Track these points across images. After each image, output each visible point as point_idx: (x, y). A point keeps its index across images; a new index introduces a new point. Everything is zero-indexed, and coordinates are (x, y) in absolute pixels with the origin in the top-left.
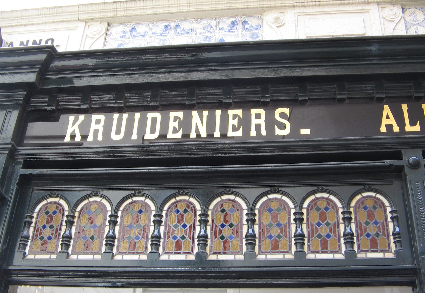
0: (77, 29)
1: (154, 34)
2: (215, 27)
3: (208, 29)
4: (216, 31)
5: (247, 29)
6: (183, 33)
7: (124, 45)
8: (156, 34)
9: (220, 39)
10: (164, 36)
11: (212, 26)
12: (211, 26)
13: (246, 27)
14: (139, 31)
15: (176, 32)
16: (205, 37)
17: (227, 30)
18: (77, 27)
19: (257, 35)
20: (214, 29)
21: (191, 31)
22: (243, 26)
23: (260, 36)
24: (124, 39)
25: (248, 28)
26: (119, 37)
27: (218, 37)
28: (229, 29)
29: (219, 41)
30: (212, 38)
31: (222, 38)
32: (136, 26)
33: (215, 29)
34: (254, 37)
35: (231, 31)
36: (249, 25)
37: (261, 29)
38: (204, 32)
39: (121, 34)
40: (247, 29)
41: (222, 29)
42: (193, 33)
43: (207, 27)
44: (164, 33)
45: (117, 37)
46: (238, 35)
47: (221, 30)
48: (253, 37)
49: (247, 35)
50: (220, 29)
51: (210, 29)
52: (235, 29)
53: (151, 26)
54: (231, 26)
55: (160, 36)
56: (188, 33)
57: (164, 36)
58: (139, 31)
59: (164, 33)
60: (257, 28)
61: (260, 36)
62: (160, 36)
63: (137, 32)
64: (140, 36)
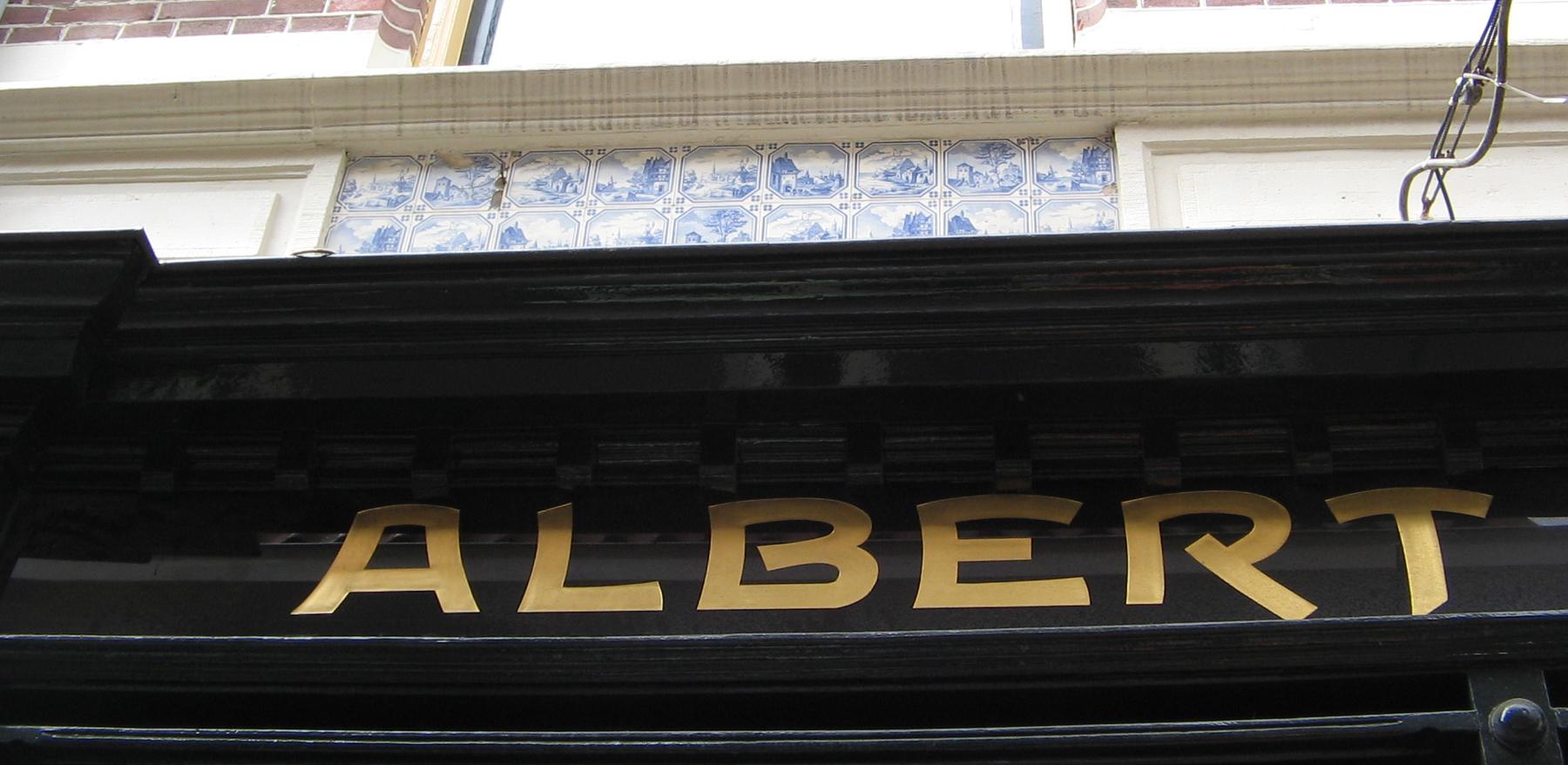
0: (305, 177)
1: (603, 194)
2: (582, 181)
3: (554, 187)
4: (584, 199)
5: (787, 188)
6: (806, 192)
7: (929, 222)
8: (614, 194)
9: (506, 231)
10: (644, 200)
11: (918, 169)
12: (914, 169)
13: (784, 182)
14: (807, 173)
15: (779, 186)
16: (715, 213)
17: (625, 195)
18: (310, 168)
19: (736, 217)
20: (926, 181)
21: (837, 182)
22: (775, 176)
23: (745, 222)
24: (399, 213)
25: (793, 187)
26: (384, 203)
27: (944, 209)
28: (635, 189)
29: (951, 230)
30: (741, 219)
31: (962, 213)
32: (791, 153)
33: (579, 191)
34: (723, 222)
35: (1084, 189)
36: (796, 174)
37: (843, 192)
38: (538, 198)
39: (390, 193)
40: (787, 188)
41: (609, 188)
42: (847, 190)
43: (550, 181)
44: (1088, 179)
45: (375, 203)
46: (577, 217)
47: (1046, 184)
48: (720, 225)
49: (695, 215)
50: (597, 190)
51: (910, 178)
52: (1100, 179)
53: (593, 162)
54: (1085, 170)
55: (628, 200)
56: (825, 191)
57: (644, 200)
58: (807, 173)
59: (645, 190)
60: (826, 186)
61: (745, 222)
62: (628, 200)
63: (799, 176)
64: (813, 190)
